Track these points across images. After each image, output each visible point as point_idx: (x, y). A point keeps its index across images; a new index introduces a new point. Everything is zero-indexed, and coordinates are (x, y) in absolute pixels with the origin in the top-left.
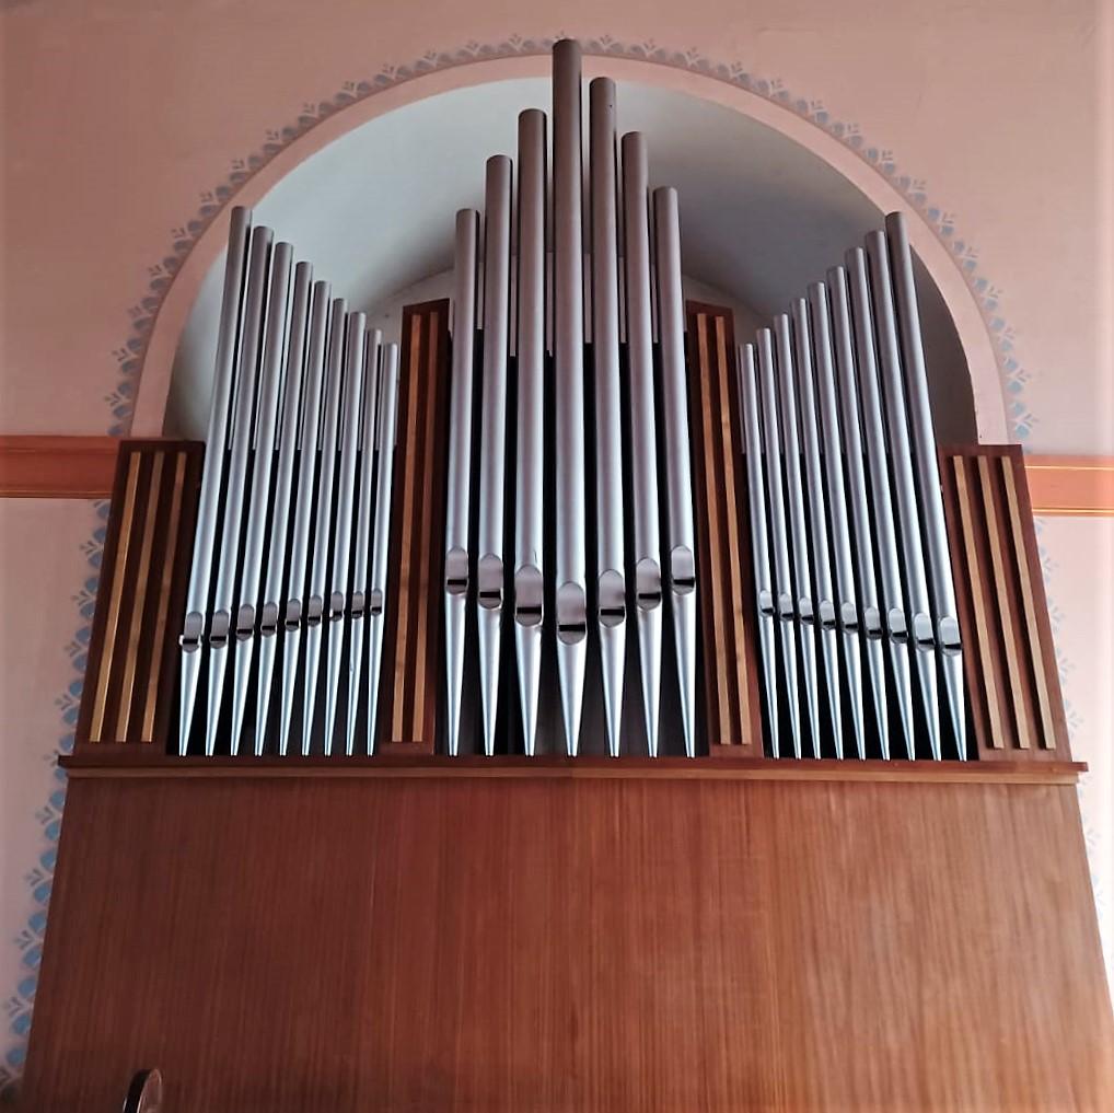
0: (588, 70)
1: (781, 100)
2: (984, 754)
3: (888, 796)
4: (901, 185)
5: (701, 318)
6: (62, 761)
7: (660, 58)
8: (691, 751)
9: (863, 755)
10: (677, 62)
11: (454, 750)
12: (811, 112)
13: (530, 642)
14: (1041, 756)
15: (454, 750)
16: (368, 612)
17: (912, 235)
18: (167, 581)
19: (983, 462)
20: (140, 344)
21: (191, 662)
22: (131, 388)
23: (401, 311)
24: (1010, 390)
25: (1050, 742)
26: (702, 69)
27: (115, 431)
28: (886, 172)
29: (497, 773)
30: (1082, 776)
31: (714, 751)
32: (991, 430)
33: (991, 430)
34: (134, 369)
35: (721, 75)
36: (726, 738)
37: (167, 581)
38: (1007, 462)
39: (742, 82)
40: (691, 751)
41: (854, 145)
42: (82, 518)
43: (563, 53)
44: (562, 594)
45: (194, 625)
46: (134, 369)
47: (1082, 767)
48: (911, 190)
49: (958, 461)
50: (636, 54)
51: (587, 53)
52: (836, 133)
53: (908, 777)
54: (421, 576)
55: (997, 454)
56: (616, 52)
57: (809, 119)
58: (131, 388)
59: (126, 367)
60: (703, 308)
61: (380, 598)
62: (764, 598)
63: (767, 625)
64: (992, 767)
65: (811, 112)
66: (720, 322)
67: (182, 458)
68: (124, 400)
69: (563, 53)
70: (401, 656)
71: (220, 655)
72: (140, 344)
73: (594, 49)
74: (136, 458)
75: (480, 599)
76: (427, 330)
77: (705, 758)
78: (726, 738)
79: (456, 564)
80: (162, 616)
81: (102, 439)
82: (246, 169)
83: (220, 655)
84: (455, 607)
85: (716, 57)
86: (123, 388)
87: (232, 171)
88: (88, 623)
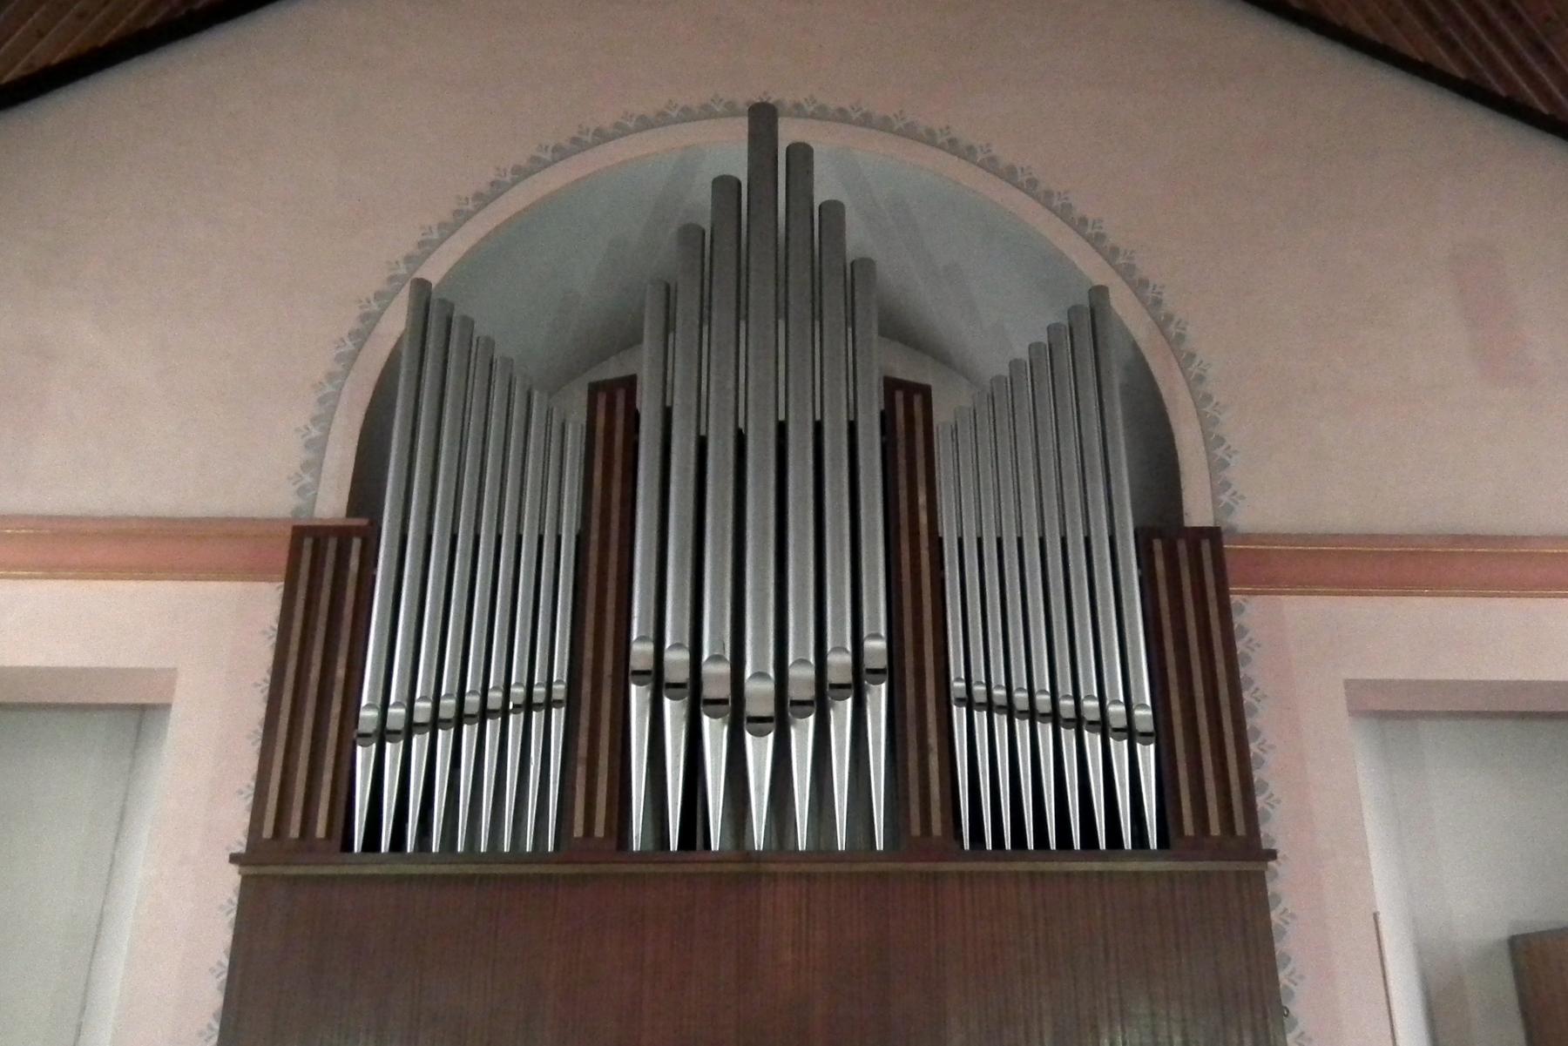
0: (789, 132)
4: (1111, 255)
5: (899, 395)
6: (1272, 855)
7: (866, 121)
9: (1053, 846)
12: (1022, 178)
13: (714, 733)
18: (340, 672)
19: (1182, 546)
21: (363, 757)
22: (314, 466)
23: (586, 389)
24: (1217, 467)
25: (1240, 829)
27: (298, 510)
28: (1096, 241)
29: (678, 869)
30: (1271, 864)
32: (1198, 512)
33: (1198, 512)
35: (929, 139)
37: (340, 672)
38: (1206, 546)
42: (263, 601)
43: (763, 118)
44: (752, 686)
47: (234, 859)
48: (1120, 260)
50: (842, 116)
51: (789, 115)
52: (1046, 199)
53: (1097, 866)
55: (1201, 532)
56: (821, 114)
57: (1019, 187)
58: (314, 466)
59: (309, 445)
62: (958, 686)
65: (1022, 178)
67: (356, 543)
68: (308, 479)
69: (763, 118)
70: (582, 751)
71: (392, 751)
73: (798, 111)
74: (308, 543)
75: (664, 691)
76: (614, 405)
77: (398, 855)
79: (641, 652)
80: (336, 709)
82: (436, 236)
83: (392, 751)
86: (306, 466)
87: (420, 238)
88: (1250, 722)
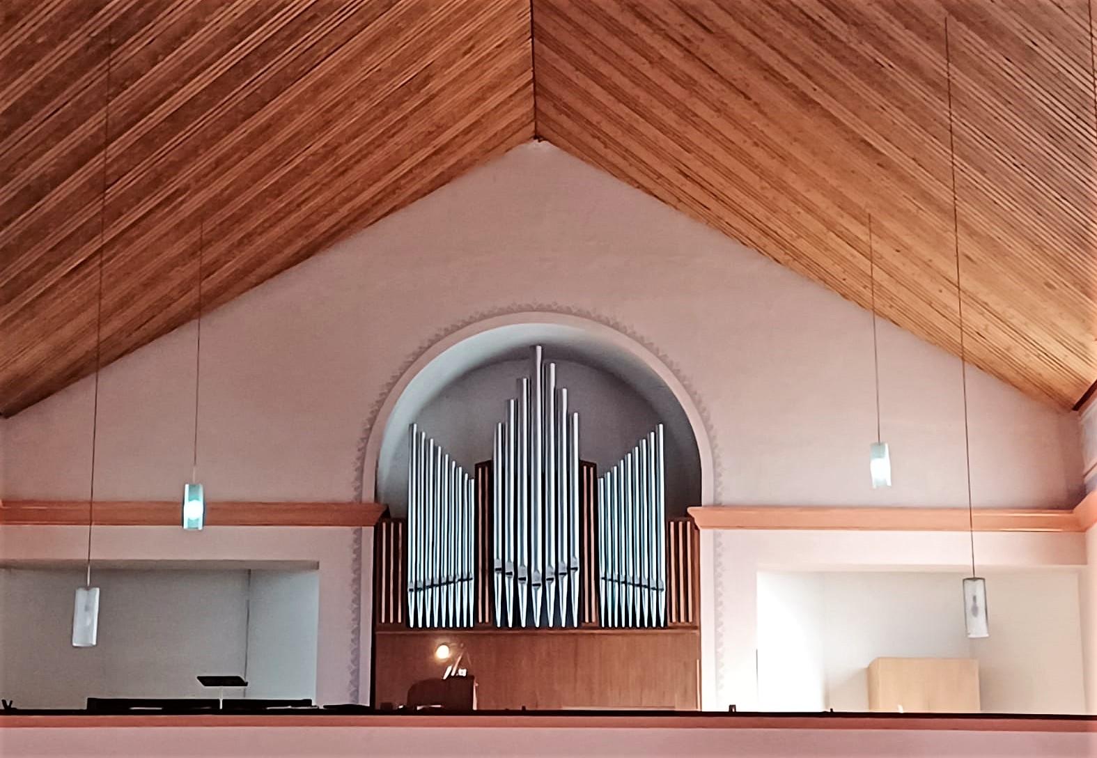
1: (632, 336)
2: (669, 624)
3: (638, 638)
8: (576, 625)
10: (587, 316)
11: (499, 625)
14: (687, 624)
15: (499, 625)
16: (468, 579)
17: (903, 28)
20: (362, 459)
25: (690, 620)
26: (598, 319)
31: (583, 624)
34: (361, 470)
36: (587, 620)
39: (616, 327)
40: (576, 625)
41: (663, 359)
45: (411, 586)
46: (361, 470)
49: (672, 524)
53: (646, 631)
54: (485, 568)
60: (589, 465)
61: (472, 575)
62: (602, 574)
63: (602, 583)
64: (670, 628)
66: (592, 469)
72: (362, 459)
78: (587, 620)
79: (497, 564)
81: (351, 503)
84: (498, 577)
85: (605, 313)
